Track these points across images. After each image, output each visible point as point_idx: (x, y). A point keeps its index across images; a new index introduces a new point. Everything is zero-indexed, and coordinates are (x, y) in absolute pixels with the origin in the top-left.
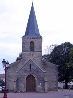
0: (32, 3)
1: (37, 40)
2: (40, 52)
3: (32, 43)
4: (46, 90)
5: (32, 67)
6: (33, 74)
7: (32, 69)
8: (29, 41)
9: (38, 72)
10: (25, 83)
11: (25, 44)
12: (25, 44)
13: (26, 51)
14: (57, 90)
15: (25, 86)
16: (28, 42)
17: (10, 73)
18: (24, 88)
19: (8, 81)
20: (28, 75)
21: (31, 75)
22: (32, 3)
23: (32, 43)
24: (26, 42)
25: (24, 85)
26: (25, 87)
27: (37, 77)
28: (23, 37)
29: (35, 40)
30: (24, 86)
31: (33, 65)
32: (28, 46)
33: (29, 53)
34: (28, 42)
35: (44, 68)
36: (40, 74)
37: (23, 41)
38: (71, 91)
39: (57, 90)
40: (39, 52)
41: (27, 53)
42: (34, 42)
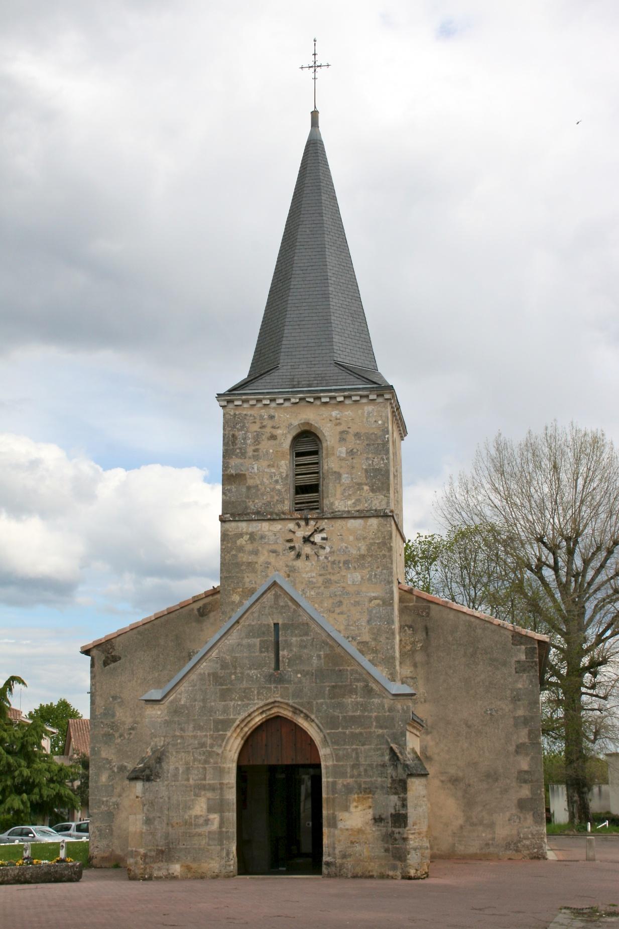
0: (315, 115)
1: (348, 413)
2: (374, 522)
3: (307, 443)
4: (413, 859)
5: (289, 645)
6: (296, 711)
7: (291, 661)
8: (288, 420)
9: (339, 691)
10: (231, 795)
11: (243, 454)
12: (243, 454)
13: (258, 513)
14: (105, 655)
15: (232, 816)
16: (273, 437)
17: (122, 704)
18: (221, 836)
19: (104, 778)
20: (258, 720)
21: (278, 718)
22: (315, 115)
23: (307, 443)
24: (257, 439)
25: (217, 807)
26: (233, 829)
27: (334, 740)
28: (228, 398)
29: (335, 413)
30: (222, 823)
31: (303, 627)
32: (274, 471)
33: (278, 526)
34: (273, 437)
35: (419, 657)
36: (364, 707)
37: (226, 424)
38: (33, 545)
39: (105, 655)
40: (363, 515)
41: (265, 526)
42: (329, 434)
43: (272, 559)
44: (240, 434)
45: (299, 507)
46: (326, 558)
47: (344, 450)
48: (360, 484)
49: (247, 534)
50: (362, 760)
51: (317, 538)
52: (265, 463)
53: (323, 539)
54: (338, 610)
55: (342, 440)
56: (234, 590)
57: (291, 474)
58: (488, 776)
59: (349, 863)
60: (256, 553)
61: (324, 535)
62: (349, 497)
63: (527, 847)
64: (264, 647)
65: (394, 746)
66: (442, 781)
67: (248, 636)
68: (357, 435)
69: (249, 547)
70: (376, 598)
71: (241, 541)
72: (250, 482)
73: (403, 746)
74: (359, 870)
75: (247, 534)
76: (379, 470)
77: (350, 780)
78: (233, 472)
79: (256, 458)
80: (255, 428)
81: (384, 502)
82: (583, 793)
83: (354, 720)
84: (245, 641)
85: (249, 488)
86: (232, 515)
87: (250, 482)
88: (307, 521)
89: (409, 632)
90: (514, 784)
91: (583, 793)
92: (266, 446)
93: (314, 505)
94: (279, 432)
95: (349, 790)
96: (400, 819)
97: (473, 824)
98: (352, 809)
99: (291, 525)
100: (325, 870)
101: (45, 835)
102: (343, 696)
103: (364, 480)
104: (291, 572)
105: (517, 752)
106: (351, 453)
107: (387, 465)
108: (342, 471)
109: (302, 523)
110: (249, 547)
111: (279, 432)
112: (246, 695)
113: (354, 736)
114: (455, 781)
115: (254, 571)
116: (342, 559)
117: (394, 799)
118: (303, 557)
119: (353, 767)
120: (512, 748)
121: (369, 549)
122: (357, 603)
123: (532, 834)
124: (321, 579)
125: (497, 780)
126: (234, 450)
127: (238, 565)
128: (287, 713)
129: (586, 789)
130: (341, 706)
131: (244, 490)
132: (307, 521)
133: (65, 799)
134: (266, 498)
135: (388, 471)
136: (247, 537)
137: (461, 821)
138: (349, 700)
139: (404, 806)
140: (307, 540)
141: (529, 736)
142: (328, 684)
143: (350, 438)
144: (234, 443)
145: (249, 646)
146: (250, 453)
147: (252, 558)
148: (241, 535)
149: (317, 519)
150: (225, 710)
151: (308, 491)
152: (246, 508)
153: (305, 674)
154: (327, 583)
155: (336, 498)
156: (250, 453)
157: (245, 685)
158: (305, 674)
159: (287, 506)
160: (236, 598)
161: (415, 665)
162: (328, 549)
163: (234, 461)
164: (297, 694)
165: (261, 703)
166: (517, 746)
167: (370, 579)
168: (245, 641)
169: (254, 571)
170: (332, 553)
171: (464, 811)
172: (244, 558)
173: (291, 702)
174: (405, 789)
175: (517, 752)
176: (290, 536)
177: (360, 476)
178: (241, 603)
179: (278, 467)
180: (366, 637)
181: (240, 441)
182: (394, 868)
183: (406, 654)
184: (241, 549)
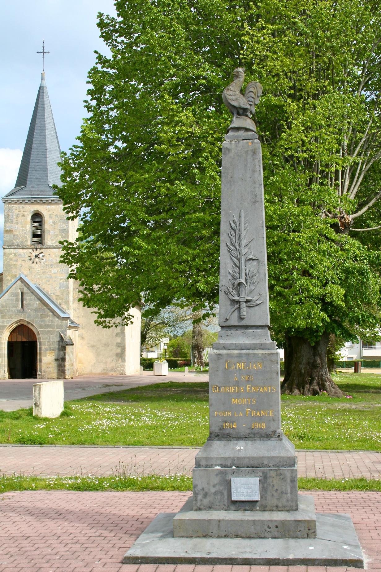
0: (41, 90)
11: (12, 222)
12: (12, 222)
16: (24, 215)
20: (15, 326)
23: (37, 218)
34: (24, 215)
43: (23, 263)
44: (11, 214)
45: (34, 243)
47: (51, 221)
48: (57, 235)
50: (51, 340)
51: (41, 256)
52: (21, 226)
53: (43, 256)
54: (48, 283)
55: (51, 217)
56: (8, 275)
57: (30, 230)
58: (105, 345)
59: (46, 374)
60: (17, 261)
61: (43, 254)
62: (53, 240)
63: (119, 371)
64: (17, 300)
65: (62, 335)
67: (11, 296)
68: (56, 216)
69: (14, 259)
71: (11, 256)
72: (15, 233)
73: (66, 335)
74: (50, 377)
76: (65, 229)
77: (47, 346)
78: (8, 229)
79: (17, 223)
80: (17, 211)
82: (200, 352)
83: (48, 326)
84: (10, 298)
85: (14, 235)
86: (8, 246)
87: (15, 233)
88: (37, 249)
91: (200, 352)
92: (21, 219)
93: (42, 243)
94: (26, 213)
95: (46, 350)
96: (63, 360)
97: (99, 362)
98: (48, 356)
99: (31, 250)
100: (38, 377)
101: (334, 234)
102: (45, 317)
103: (59, 233)
104: (30, 268)
105: (116, 336)
106: (54, 222)
107: (68, 228)
108: (50, 230)
109: (35, 250)
110: (14, 259)
111: (26, 213)
112: (11, 317)
113: (48, 331)
114: (93, 346)
115: (16, 268)
116: (50, 264)
117: (62, 352)
118: (35, 263)
119: (48, 342)
120: (114, 334)
122: (55, 281)
124: (42, 271)
125: (108, 346)
126: (8, 220)
127: (10, 265)
128: (25, 324)
129: (201, 350)
130: (44, 321)
131: (12, 236)
132: (37, 249)
134: (21, 240)
135: (68, 230)
137: (95, 361)
138: (47, 319)
139: (65, 355)
140: (36, 256)
142: (39, 314)
143: (54, 217)
144: (8, 218)
145: (12, 300)
146: (15, 222)
147: (15, 263)
148: (11, 254)
149: (40, 249)
150: (3, 322)
151: (38, 237)
152: (13, 243)
153: (32, 310)
154: (44, 273)
156: (15, 222)
157: (10, 313)
158: (32, 310)
159: (29, 243)
160: (9, 278)
162: (44, 260)
163: (8, 225)
164: (29, 317)
165: (16, 320)
167: (60, 272)
168: (10, 298)
169: (16, 268)
170: (46, 261)
172: (12, 262)
173: (26, 320)
174: (65, 349)
175: (116, 336)
176: (30, 255)
177: (57, 232)
178: (11, 280)
179: (26, 228)
180: (59, 294)
181: (10, 216)
182: (61, 376)
184: (11, 259)
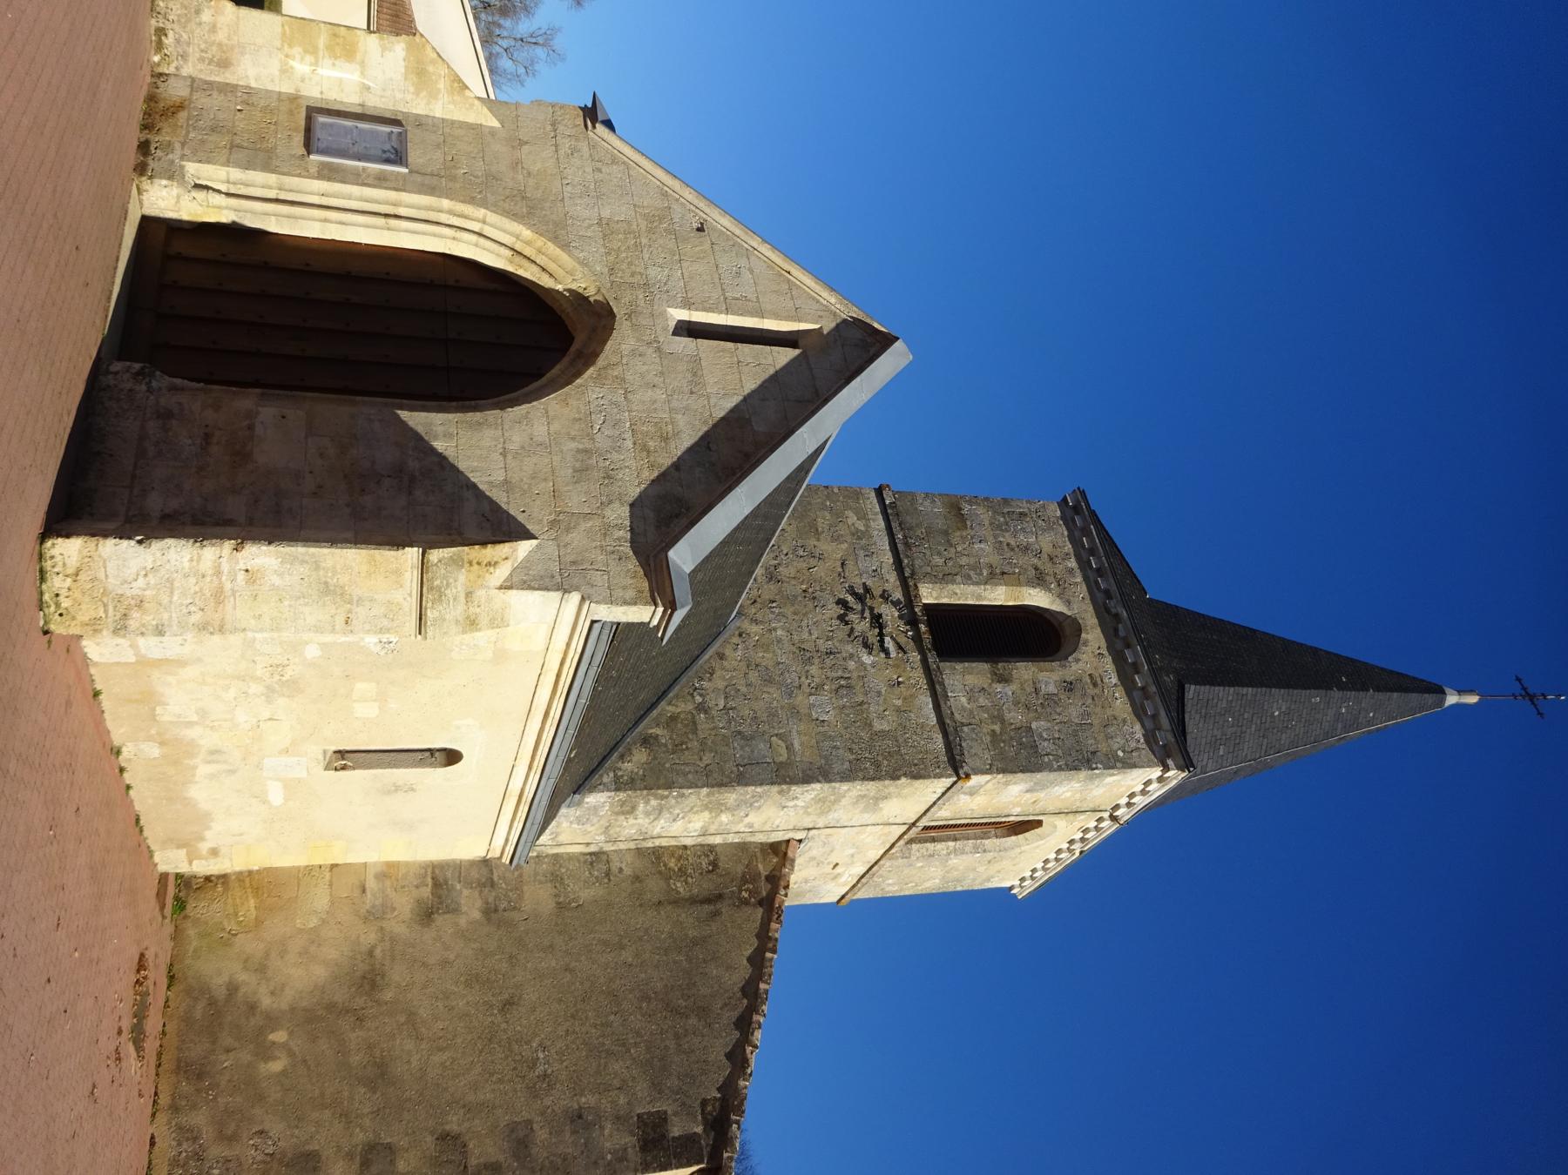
35: (654, 886)
44: (1029, 526)
46: (851, 656)
49: (867, 526)
66: (371, 953)
70: (789, 748)
75: (867, 526)
81: (978, 764)
85: (946, 533)
89: (704, 862)
90: (360, 1137)
120: (453, 1124)
121: (883, 734)
123: (608, 254)
133: (143, 847)
136: (860, 526)
141: (486, 1166)
146: (1007, 538)
155: (966, 681)
161: (637, 878)
166: (456, 1137)
171: (293, 1009)
183: (658, 858)
184: (839, 516)
